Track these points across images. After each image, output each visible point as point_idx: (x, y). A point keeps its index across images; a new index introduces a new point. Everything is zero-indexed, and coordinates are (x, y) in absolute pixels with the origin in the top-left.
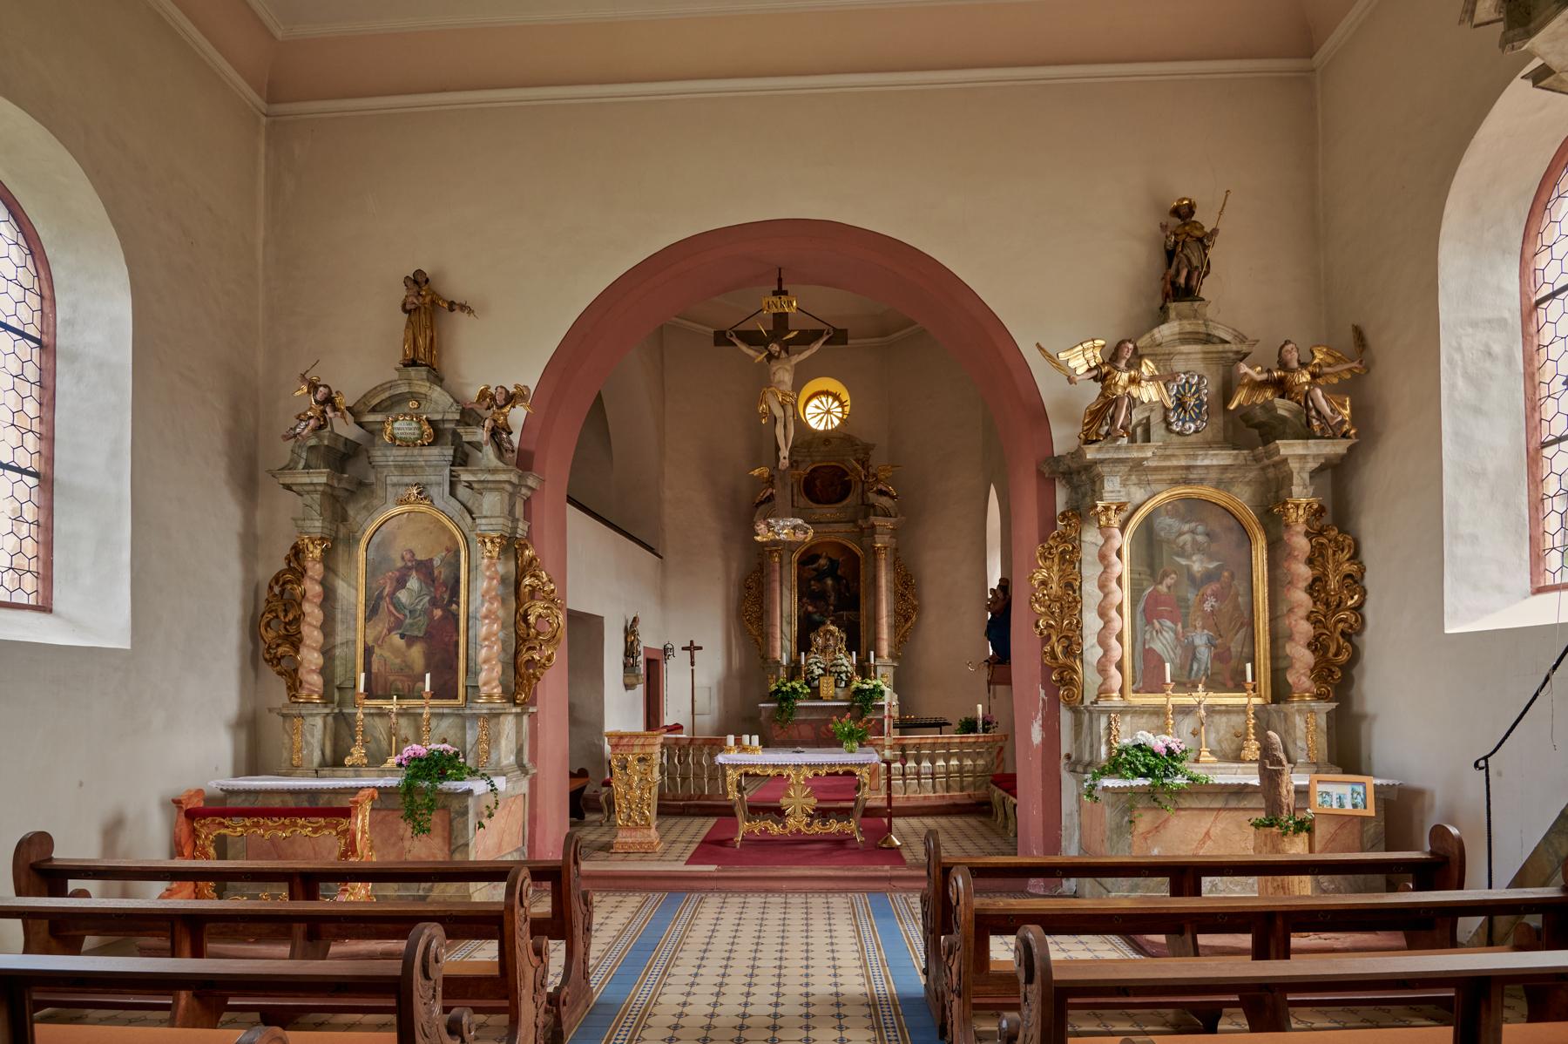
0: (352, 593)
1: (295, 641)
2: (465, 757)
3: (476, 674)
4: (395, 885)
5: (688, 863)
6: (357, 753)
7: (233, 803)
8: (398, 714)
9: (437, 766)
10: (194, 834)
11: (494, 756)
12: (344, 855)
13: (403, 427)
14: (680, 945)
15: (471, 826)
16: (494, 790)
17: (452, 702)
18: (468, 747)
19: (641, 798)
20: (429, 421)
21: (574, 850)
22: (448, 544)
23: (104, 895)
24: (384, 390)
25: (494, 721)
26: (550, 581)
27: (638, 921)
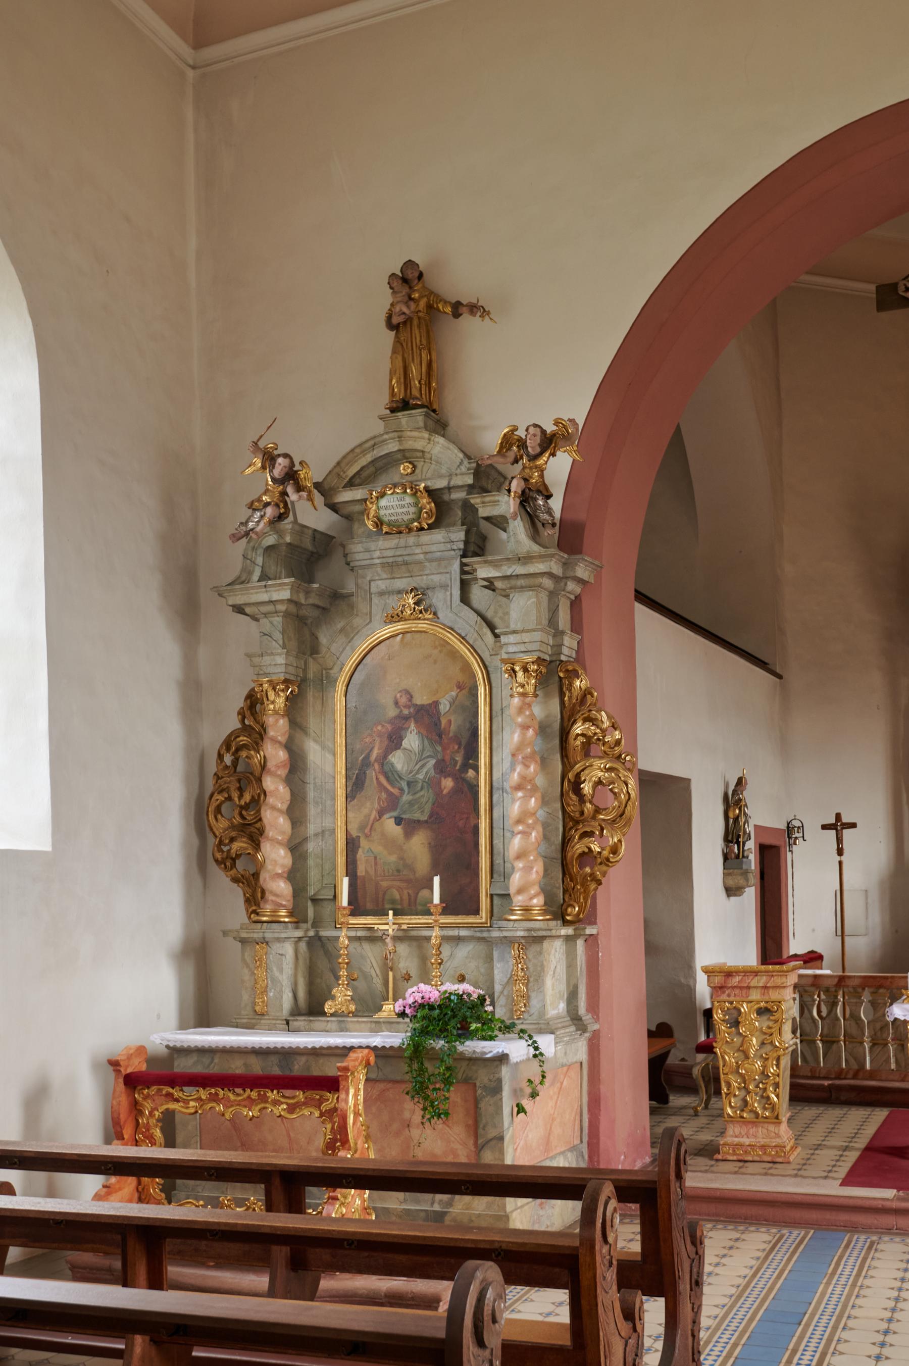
0: (328, 761)
1: (253, 832)
2: (492, 1003)
3: (506, 876)
4: (401, 1195)
5: (845, 1183)
6: (341, 997)
7: (183, 1066)
8: (396, 939)
9: (454, 1018)
10: (136, 1108)
11: (535, 1003)
12: (331, 1146)
13: (394, 505)
14: (841, 1320)
15: (506, 1110)
16: (538, 1055)
17: (471, 919)
18: (498, 988)
19: (764, 1074)
20: (429, 492)
21: (672, 1154)
22: (460, 677)
23: (29, 1192)
24: (364, 452)
25: (534, 948)
26: (614, 727)
27: (768, 1274)
